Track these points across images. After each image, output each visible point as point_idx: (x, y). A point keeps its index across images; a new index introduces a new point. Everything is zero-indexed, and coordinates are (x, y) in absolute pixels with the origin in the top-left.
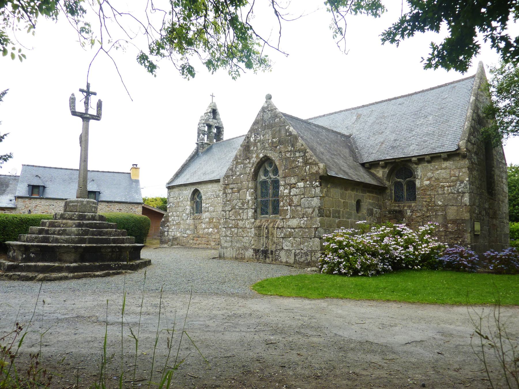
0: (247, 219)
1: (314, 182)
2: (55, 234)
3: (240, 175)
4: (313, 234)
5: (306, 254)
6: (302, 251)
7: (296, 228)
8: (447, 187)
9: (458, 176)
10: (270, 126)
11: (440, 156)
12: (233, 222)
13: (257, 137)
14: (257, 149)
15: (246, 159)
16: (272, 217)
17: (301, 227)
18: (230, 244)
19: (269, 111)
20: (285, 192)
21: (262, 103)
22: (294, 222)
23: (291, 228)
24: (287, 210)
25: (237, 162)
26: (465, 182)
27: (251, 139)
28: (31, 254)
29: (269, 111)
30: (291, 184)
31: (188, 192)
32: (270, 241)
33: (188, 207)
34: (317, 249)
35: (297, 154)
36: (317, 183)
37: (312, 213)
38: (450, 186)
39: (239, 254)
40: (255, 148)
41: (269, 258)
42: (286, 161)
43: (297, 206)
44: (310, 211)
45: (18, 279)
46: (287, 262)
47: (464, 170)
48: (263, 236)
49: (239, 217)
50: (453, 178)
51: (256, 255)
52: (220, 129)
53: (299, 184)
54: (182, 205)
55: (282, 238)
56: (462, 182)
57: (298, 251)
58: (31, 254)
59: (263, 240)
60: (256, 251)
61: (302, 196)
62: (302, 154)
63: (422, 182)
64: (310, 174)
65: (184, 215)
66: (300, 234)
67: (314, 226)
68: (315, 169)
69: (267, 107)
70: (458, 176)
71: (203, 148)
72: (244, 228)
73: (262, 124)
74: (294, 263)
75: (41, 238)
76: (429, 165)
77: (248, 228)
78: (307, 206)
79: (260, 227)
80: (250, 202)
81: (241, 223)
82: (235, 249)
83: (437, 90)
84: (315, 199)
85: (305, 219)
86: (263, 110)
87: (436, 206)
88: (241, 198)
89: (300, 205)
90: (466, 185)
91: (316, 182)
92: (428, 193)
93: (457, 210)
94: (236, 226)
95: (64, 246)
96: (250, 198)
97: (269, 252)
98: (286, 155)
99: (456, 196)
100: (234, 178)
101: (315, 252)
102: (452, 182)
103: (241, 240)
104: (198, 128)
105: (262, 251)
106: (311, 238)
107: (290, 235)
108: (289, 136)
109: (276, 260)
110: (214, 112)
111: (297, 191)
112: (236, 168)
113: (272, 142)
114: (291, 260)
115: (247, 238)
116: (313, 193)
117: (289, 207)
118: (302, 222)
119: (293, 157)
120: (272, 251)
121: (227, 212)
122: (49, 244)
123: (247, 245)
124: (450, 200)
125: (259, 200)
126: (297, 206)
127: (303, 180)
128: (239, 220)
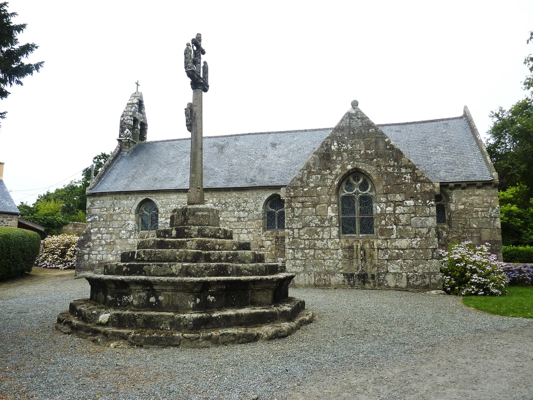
0: (330, 238)
1: (428, 201)
2: (221, 261)
3: (316, 187)
4: (431, 255)
5: (423, 276)
6: (417, 274)
7: (407, 249)
8: (481, 212)
9: (490, 203)
10: (362, 136)
11: (476, 184)
12: (307, 242)
13: (342, 146)
14: (342, 160)
15: (325, 170)
16: (362, 237)
17: (414, 248)
18: (302, 268)
19: (358, 118)
20: (387, 209)
21: (348, 108)
22: (404, 243)
23: (399, 249)
24: (392, 229)
25: (309, 172)
26: (497, 208)
27: (333, 147)
28: (209, 297)
29: (358, 118)
30: (396, 202)
31: (133, 203)
32: (368, 264)
33: (130, 222)
34: (435, 270)
35: (403, 170)
36: (433, 203)
37: (428, 233)
38: (483, 211)
39: (320, 280)
40: (340, 158)
41: (369, 283)
42: (387, 176)
43: (406, 225)
44: (425, 231)
45: (233, 342)
46: (396, 287)
47: (495, 198)
48: (357, 258)
49: (316, 237)
50: (485, 204)
51: (349, 281)
52: (144, 126)
53: (408, 202)
54: (120, 219)
55: (387, 260)
56: (494, 208)
57: (411, 274)
58: (209, 297)
59: (357, 263)
60: (349, 276)
61: (412, 215)
62: (410, 170)
63: (456, 205)
64: (421, 192)
65: (123, 232)
66: (413, 255)
67: (431, 247)
68: (428, 188)
69: (356, 114)
70: (490, 203)
71: (129, 147)
72: (325, 250)
73: (349, 132)
74: (407, 287)
75: (215, 267)
76: (463, 191)
77: (333, 250)
78: (419, 225)
79: (351, 248)
80: (334, 219)
81: (319, 244)
82: (312, 275)
83: (430, 123)
84: (430, 218)
85: (418, 239)
86: (349, 115)
87: (471, 228)
88: (318, 214)
89: (410, 225)
90: (497, 211)
91: (431, 201)
92: (464, 216)
93: (491, 232)
94: (313, 247)
95: (267, 279)
96: (333, 215)
97: (369, 276)
98: (387, 170)
99: (489, 220)
100: (305, 190)
101: (435, 274)
102: (485, 207)
103: (321, 264)
104: (122, 122)
105: (358, 275)
106: (427, 260)
107: (398, 257)
108: (390, 149)
109: (380, 285)
110: (140, 104)
111: (406, 209)
112: (308, 178)
113: (366, 154)
114: (403, 283)
115: (331, 261)
116: (428, 212)
117: (394, 227)
118: (414, 243)
119: (397, 173)
120: (373, 277)
121: (296, 231)
122: (243, 278)
123: (332, 269)
124: (484, 223)
125: (341, 217)
126: (406, 225)
127: (412, 197)
128: (318, 240)
